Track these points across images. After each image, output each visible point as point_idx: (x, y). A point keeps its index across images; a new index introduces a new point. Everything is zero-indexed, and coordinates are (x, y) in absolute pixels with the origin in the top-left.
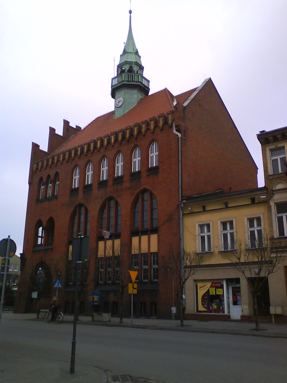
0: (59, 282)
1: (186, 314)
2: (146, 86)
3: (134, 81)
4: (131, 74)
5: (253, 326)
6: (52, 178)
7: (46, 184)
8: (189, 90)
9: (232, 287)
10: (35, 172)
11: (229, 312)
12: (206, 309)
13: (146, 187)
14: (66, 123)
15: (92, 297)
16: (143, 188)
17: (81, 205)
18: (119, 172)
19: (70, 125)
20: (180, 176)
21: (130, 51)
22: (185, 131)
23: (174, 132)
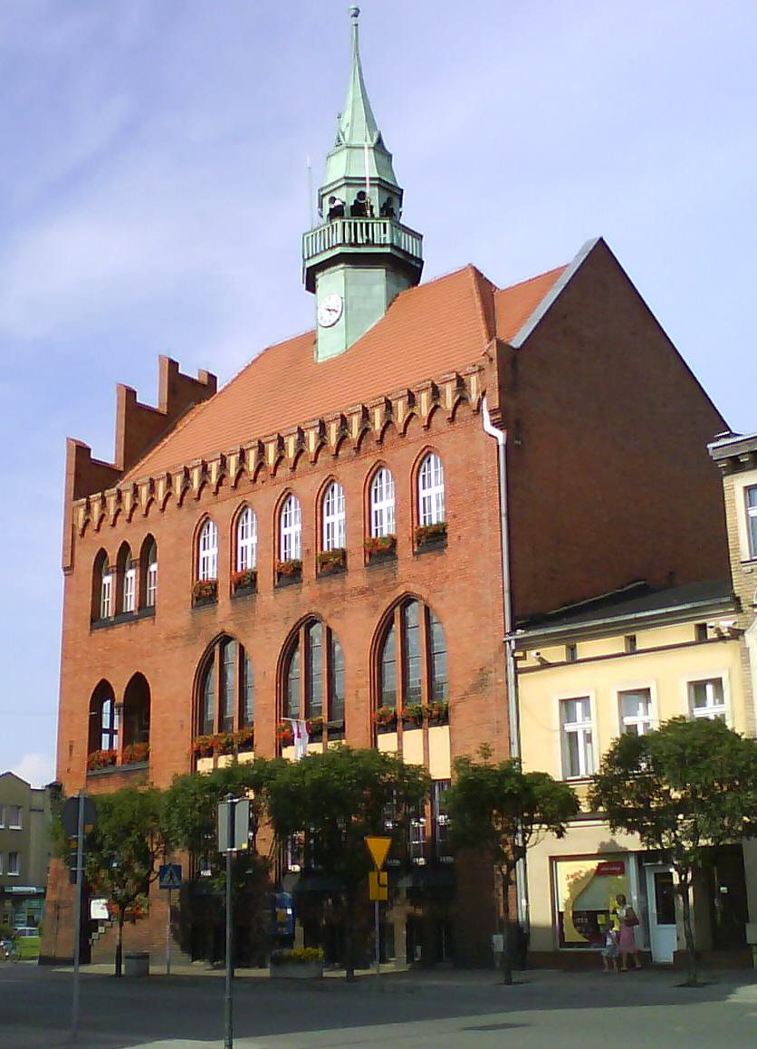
1: (534, 953)
2: (412, 255)
3: (373, 245)
4: (361, 221)
5: (683, 978)
6: (136, 552)
7: (120, 571)
8: (541, 273)
9: (655, 874)
11: (648, 944)
12: (585, 937)
13: (415, 589)
15: (270, 911)
16: (403, 591)
17: (225, 639)
19: (180, 371)
23: (486, 429)
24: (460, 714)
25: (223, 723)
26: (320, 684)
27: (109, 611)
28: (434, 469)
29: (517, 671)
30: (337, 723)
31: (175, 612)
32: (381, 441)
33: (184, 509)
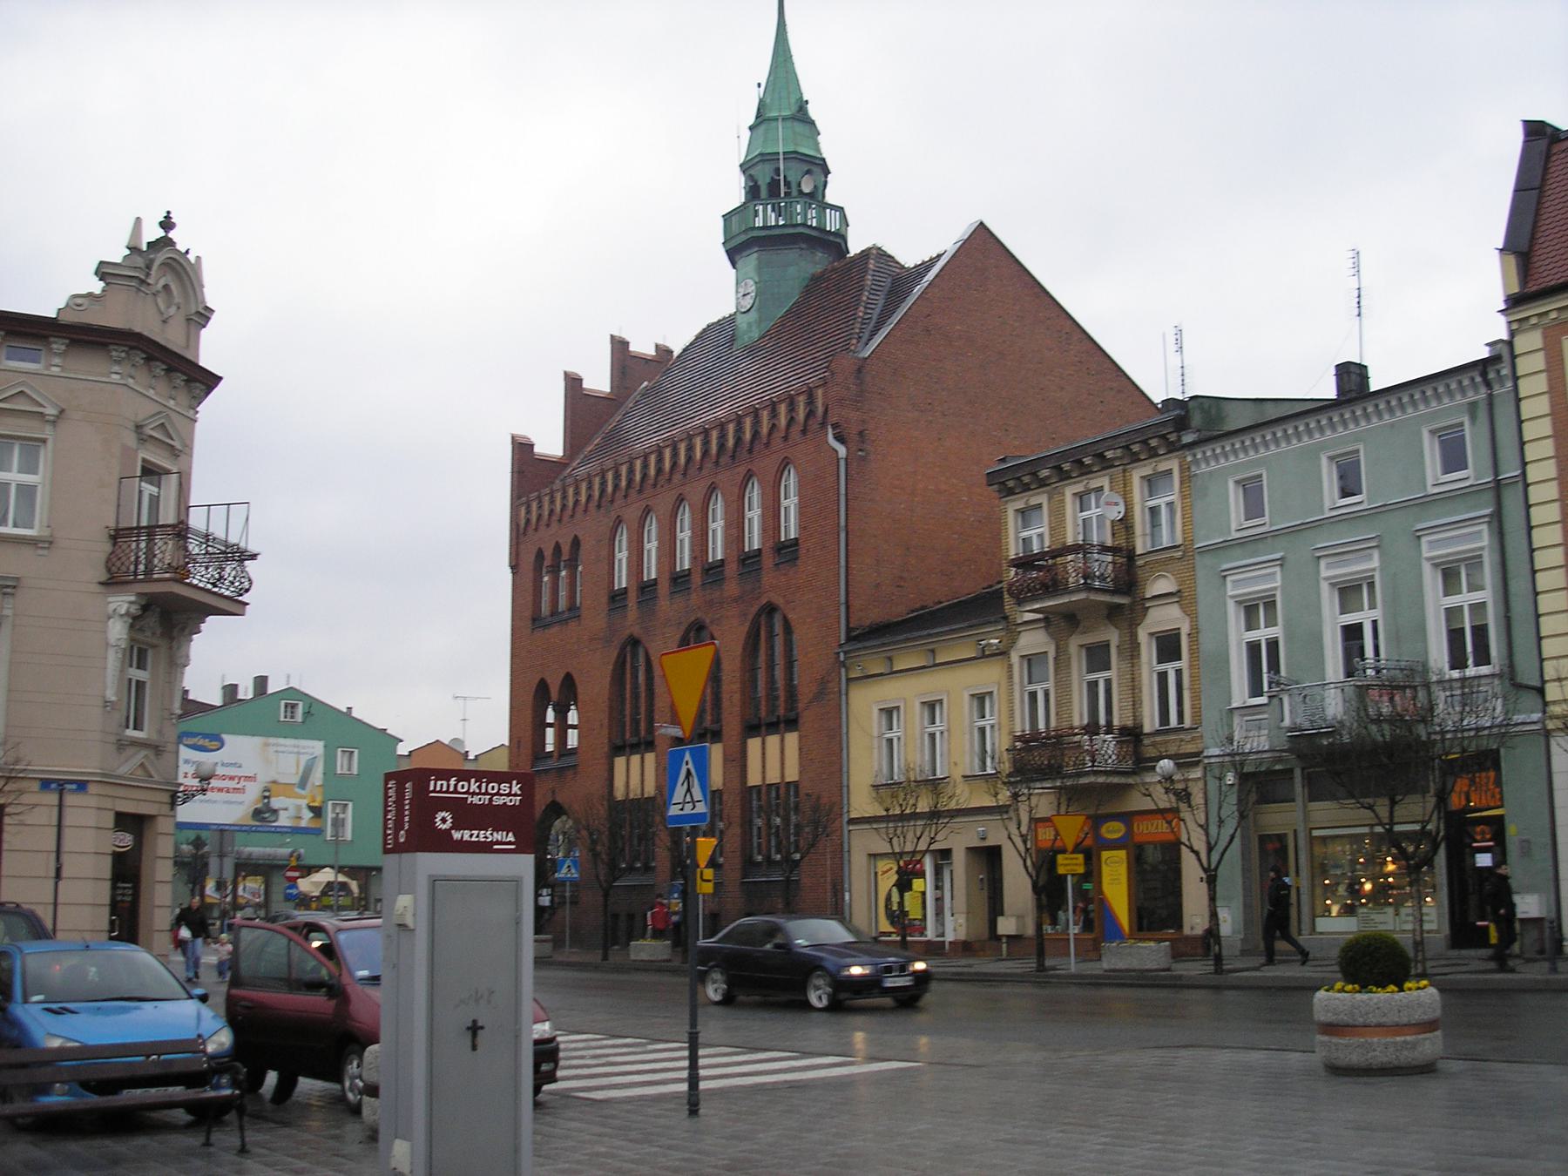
0: (693, 771)
6: (566, 549)
7: (555, 570)
10: (525, 534)
14: (619, 346)
17: (634, 642)
18: (717, 551)
20: (843, 571)
21: (783, 114)
22: (861, 433)
24: (807, 718)
25: (772, 698)
26: (779, 673)
27: (545, 609)
28: (791, 480)
29: (849, 680)
30: (792, 715)
31: (595, 618)
32: (750, 451)
33: (602, 510)
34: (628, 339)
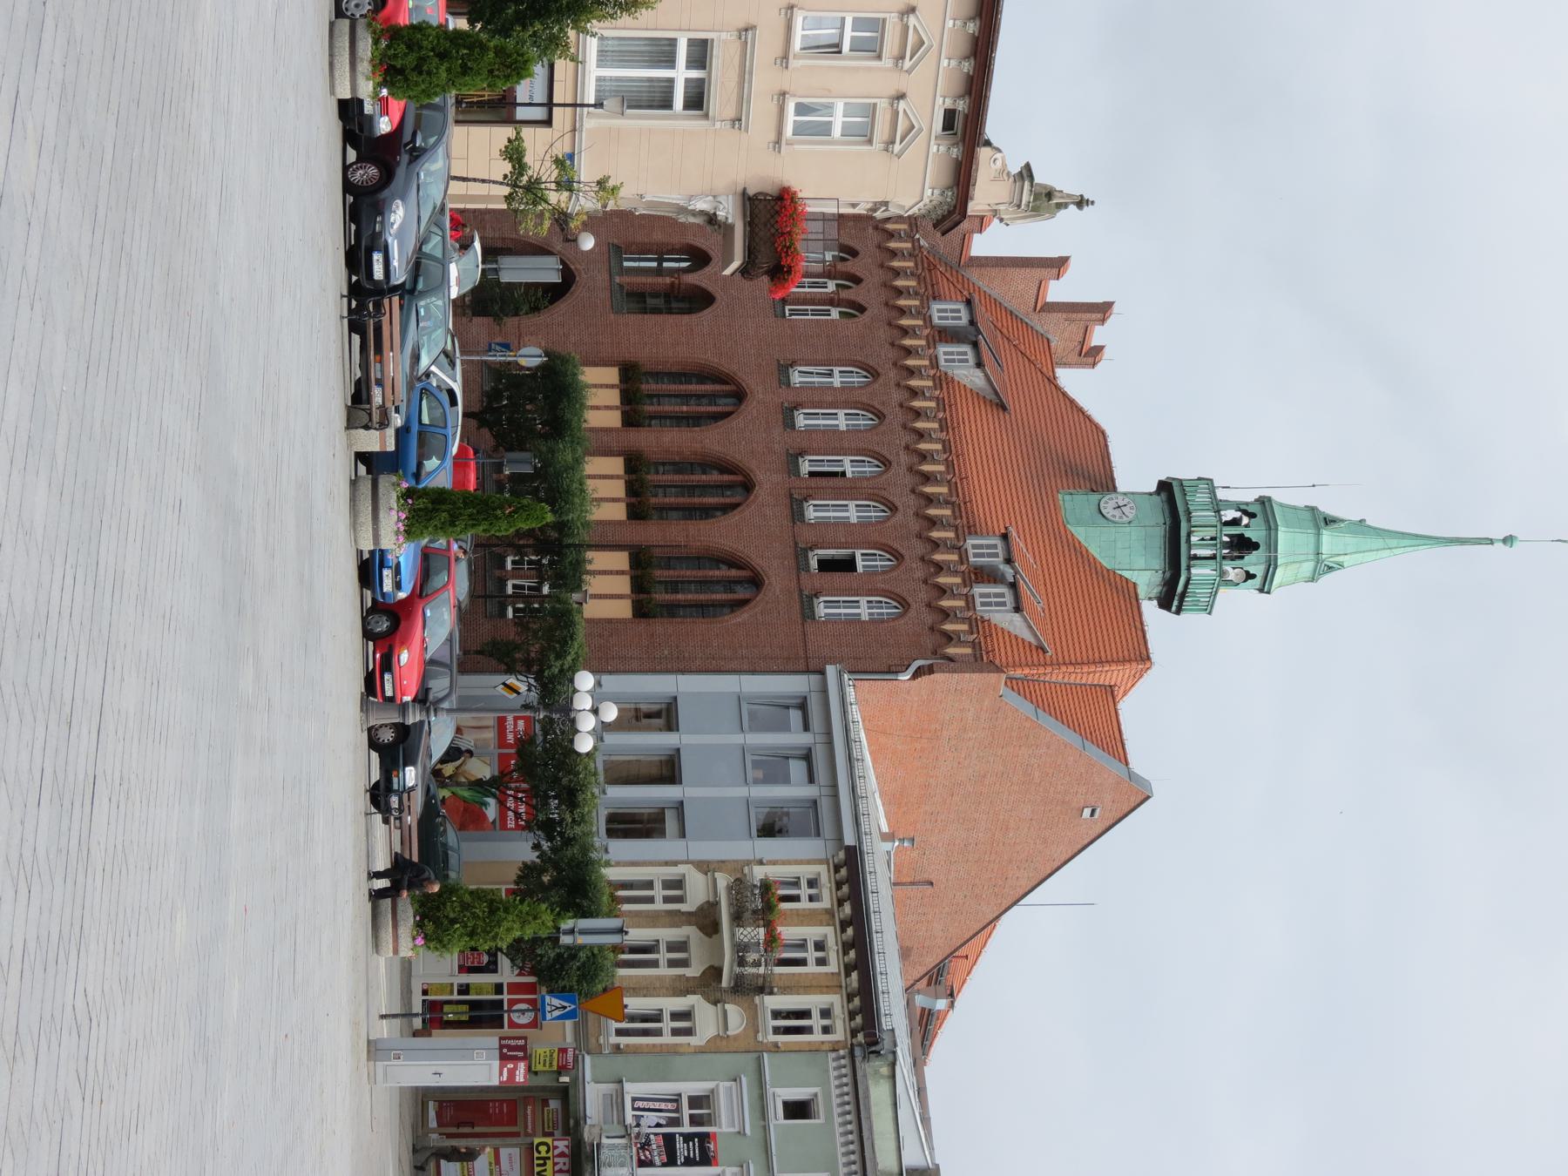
14: (1102, 310)
24: (642, 625)
34: (1109, 322)
